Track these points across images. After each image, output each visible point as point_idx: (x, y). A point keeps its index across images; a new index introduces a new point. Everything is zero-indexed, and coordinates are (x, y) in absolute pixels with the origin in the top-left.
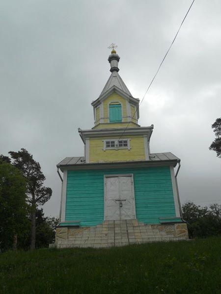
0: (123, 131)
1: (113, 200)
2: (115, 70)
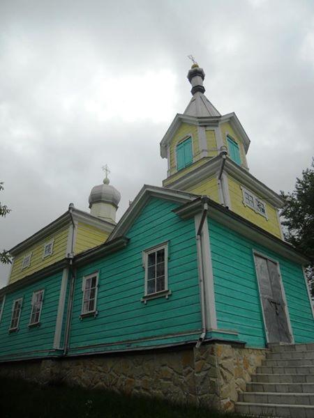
2: (198, 90)
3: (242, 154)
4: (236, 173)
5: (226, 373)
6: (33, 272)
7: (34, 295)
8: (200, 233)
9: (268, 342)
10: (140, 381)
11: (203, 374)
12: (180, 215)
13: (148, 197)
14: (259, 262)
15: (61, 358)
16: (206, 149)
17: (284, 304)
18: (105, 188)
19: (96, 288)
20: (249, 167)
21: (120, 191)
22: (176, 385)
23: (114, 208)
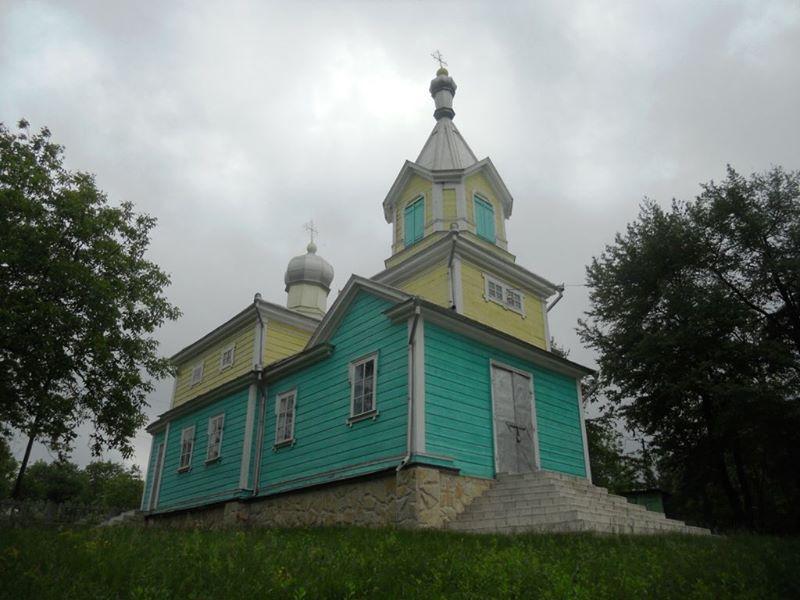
0: (543, 285)
1: (506, 423)
2: (444, 113)
3: (499, 219)
4: (476, 256)
5: (427, 498)
6: (208, 390)
7: (211, 421)
8: (412, 342)
9: (497, 471)
10: (342, 515)
11: (403, 499)
12: (393, 318)
13: (357, 290)
14: (499, 377)
15: (250, 500)
16: (441, 218)
17: (532, 429)
18: (310, 261)
19: (294, 410)
20: (507, 239)
21: (332, 264)
22: (378, 514)
23: (325, 293)
